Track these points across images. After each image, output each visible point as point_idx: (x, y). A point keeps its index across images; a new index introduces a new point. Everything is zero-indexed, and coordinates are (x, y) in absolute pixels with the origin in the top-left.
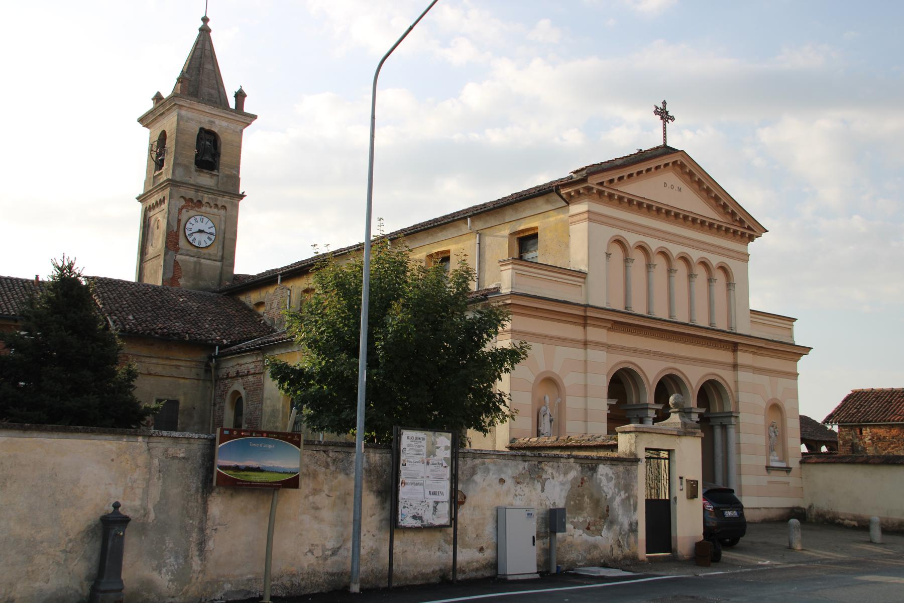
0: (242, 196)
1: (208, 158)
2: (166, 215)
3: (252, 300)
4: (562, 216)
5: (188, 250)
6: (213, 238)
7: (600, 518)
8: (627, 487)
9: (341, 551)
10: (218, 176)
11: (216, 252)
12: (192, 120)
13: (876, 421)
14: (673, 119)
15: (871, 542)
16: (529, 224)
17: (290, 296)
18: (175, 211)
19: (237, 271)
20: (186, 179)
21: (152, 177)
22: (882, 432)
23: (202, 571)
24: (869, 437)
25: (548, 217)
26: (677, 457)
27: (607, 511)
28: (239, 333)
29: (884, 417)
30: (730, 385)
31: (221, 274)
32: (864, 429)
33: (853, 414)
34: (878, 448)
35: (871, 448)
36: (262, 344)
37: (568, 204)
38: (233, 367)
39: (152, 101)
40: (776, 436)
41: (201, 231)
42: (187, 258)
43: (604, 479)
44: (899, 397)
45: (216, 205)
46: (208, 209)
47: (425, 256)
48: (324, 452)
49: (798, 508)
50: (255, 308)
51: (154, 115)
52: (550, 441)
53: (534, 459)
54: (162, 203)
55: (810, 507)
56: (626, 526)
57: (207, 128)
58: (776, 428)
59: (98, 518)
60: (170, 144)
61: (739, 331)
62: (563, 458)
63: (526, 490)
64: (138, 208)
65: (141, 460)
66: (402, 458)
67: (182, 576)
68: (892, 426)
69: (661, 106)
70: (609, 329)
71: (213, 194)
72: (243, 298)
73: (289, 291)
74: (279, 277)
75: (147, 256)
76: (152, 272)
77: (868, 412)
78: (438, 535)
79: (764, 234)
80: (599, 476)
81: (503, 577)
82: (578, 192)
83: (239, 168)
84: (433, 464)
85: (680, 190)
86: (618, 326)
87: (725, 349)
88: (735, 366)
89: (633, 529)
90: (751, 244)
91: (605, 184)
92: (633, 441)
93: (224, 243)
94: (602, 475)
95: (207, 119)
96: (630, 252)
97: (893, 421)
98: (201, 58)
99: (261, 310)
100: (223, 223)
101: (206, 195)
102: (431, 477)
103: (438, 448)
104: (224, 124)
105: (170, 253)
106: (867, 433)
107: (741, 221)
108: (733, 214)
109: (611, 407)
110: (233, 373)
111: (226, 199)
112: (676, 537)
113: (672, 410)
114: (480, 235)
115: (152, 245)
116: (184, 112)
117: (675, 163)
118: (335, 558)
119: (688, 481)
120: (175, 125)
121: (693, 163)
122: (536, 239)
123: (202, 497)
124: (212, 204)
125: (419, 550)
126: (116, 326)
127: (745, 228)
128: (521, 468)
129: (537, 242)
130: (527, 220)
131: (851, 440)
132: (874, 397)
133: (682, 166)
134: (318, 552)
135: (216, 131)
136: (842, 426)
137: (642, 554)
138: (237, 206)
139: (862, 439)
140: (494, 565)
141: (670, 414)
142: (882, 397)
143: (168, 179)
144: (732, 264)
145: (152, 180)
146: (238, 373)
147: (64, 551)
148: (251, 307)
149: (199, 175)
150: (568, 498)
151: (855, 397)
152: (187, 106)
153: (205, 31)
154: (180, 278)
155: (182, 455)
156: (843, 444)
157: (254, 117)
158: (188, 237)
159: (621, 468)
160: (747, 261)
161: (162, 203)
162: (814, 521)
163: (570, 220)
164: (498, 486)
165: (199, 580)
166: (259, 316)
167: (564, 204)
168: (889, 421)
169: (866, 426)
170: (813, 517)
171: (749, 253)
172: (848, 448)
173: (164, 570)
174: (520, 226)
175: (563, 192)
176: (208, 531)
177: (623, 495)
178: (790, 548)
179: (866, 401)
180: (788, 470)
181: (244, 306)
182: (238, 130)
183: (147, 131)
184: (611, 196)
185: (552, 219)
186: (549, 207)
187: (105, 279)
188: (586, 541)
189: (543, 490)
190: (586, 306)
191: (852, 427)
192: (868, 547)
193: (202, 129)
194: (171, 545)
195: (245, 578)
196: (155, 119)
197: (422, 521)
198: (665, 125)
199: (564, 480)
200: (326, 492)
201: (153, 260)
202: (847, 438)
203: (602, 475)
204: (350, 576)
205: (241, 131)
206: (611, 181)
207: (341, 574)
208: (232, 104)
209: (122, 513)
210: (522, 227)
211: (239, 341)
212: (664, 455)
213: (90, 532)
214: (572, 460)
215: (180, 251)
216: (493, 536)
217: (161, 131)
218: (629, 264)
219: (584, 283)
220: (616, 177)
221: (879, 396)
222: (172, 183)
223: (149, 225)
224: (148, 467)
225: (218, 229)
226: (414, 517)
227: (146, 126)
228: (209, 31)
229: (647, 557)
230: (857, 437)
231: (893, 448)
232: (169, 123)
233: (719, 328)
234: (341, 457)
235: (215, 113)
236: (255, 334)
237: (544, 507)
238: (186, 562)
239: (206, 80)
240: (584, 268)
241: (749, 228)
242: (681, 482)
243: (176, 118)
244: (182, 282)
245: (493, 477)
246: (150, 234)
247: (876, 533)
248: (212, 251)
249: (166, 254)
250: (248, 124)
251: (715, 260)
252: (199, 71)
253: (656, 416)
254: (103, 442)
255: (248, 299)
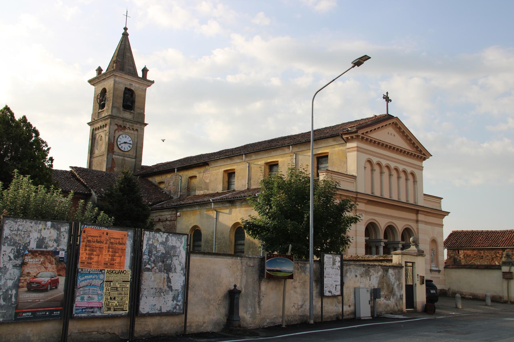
0: (146, 124)
1: (129, 103)
2: (108, 134)
3: (157, 180)
4: (342, 148)
5: (118, 153)
6: (131, 146)
7: (390, 293)
8: (399, 279)
9: (304, 306)
10: (134, 113)
11: (132, 154)
12: (121, 83)
13: (466, 247)
14: (391, 101)
15: (486, 305)
16: (323, 150)
17: (181, 179)
18: (112, 132)
19: (142, 165)
20: (118, 115)
21: (97, 112)
22: (469, 252)
23: (260, 314)
24: (463, 255)
25: (334, 148)
26: (416, 265)
27: (392, 290)
28: (155, 199)
29: (470, 245)
30: (414, 229)
31: (135, 165)
32: (460, 251)
33: (455, 243)
34: (467, 260)
35: (463, 260)
36: (176, 205)
37: (346, 142)
38: (156, 216)
39: (96, 72)
40: (434, 255)
41: (125, 143)
42: (118, 157)
43: (391, 275)
44: (476, 235)
45: (133, 129)
46: (129, 131)
47: (264, 163)
48: (297, 263)
49: (443, 290)
50: (158, 185)
51: (99, 79)
52: (347, 257)
53: (367, 266)
54: (105, 127)
55: (449, 289)
56: (399, 297)
57: (129, 88)
58: (434, 251)
59: (227, 291)
60: (109, 95)
61: (419, 204)
62: (377, 266)
63: (364, 280)
64: (88, 129)
65: (239, 267)
66: (325, 266)
67: (253, 316)
68: (474, 249)
69: (386, 94)
70: (366, 204)
71: (131, 123)
72: (150, 179)
73: (180, 177)
74: (176, 169)
75: (94, 155)
76: (98, 163)
77: (462, 242)
78: (335, 300)
79: (430, 157)
80: (389, 274)
81: (359, 318)
82: (352, 137)
83: (144, 109)
84: (335, 269)
85: (394, 136)
86: (370, 202)
87: (413, 213)
88: (417, 221)
89: (401, 298)
90: (424, 162)
91: (364, 134)
92: (400, 258)
93: (136, 149)
94: (390, 274)
95: (129, 83)
96: (374, 166)
97: (475, 247)
98: (124, 49)
99: (162, 186)
100: (136, 138)
101: (128, 124)
102: (334, 274)
103: (336, 261)
104: (137, 85)
105: (110, 154)
106: (461, 253)
107: (421, 151)
108: (417, 147)
109: (366, 241)
110: (156, 219)
111: (138, 125)
112: (416, 302)
113: (412, 244)
114: (296, 154)
115: (97, 149)
116: (117, 79)
117: (393, 123)
118: (302, 309)
119: (420, 276)
120: (112, 86)
121: (401, 123)
122: (327, 158)
123: (259, 283)
124: (131, 128)
125: (329, 306)
126: (97, 194)
127: (422, 154)
128: (362, 270)
129: (328, 160)
130: (322, 149)
131: (453, 256)
132: (464, 235)
133: (396, 124)
134: (296, 306)
135: (133, 89)
136: (449, 249)
137: (405, 309)
138: (143, 129)
139: (459, 256)
140: (354, 313)
141: (410, 246)
142: (468, 235)
143: (110, 115)
144: (416, 171)
145: (97, 114)
146: (160, 220)
147: (218, 304)
148: (156, 184)
149: (125, 113)
150: (379, 284)
151: (454, 235)
152: (119, 76)
153: (125, 35)
154: (115, 167)
155: (252, 265)
156: (450, 258)
157: (153, 82)
158: (119, 146)
159: (397, 271)
160: (422, 170)
161: (105, 127)
162: (451, 296)
163: (347, 150)
164: (354, 278)
165: (259, 317)
166: (161, 189)
167: (343, 142)
168: (473, 247)
169: (461, 249)
170: (450, 294)
171: (423, 166)
172: (452, 260)
173: (248, 313)
174: (318, 151)
175: (344, 137)
176: (261, 297)
177: (398, 282)
178: (456, 307)
179: (460, 237)
180: (439, 271)
181: (152, 184)
182: (144, 89)
183: (93, 87)
184: (363, 138)
185: (336, 149)
186: (335, 143)
187: (80, 168)
188: (385, 303)
189: (370, 280)
190: (357, 193)
191: (454, 250)
192: (486, 307)
193: (126, 88)
194: (250, 303)
195: (273, 317)
196: (99, 81)
197: (332, 294)
198: (387, 104)
199: (377, 276)
200: (298, 281)
201: (99, 157)
202: (451, 255)
203: (390, 274)
204: (310, 317)
205: (146, 89)
206: (367, 132)
207: (303, 316)
208: (140, 74)
209: (237, 289)
210: (320, 152)
211: (157, 202)
212: (410, 264)
213: (225, 296)
214: (380, 267)
215: (115, 153)
216: (353, 300)
217: (102, 88)
218: (373, 172)
219: (355, 181)
220: (369, 130)
221: (466, 234)
222: (111, 117)
223: (95, 138)
224: (242, 270)
225: (133, 141)
226: (329, 292)
227: (93, 85)
228: (128, 35)
229: (406, 310)
230: (457, 255)
231: (474, 261)
232: (109, 84)
233: (411, 203)
234: (303, 265)
235: (133, 80)
236: (163, 199)
237: (370, 287)
238: (255, 310)
239: (127, 62)
240: (355, 174)
241: (424, 154)
242: (418, 277)
243: (113, 82)
244: (115, 169)
245: (353, 274)
246: (96, 143)
247: (489, 301)
248: (131, 153)
249: (108, 155)
250: (149, 86)
251: (409, 170)
252: (124, 57)
253: (384, 245)
254: (228, 260)
255: (154, 180)
